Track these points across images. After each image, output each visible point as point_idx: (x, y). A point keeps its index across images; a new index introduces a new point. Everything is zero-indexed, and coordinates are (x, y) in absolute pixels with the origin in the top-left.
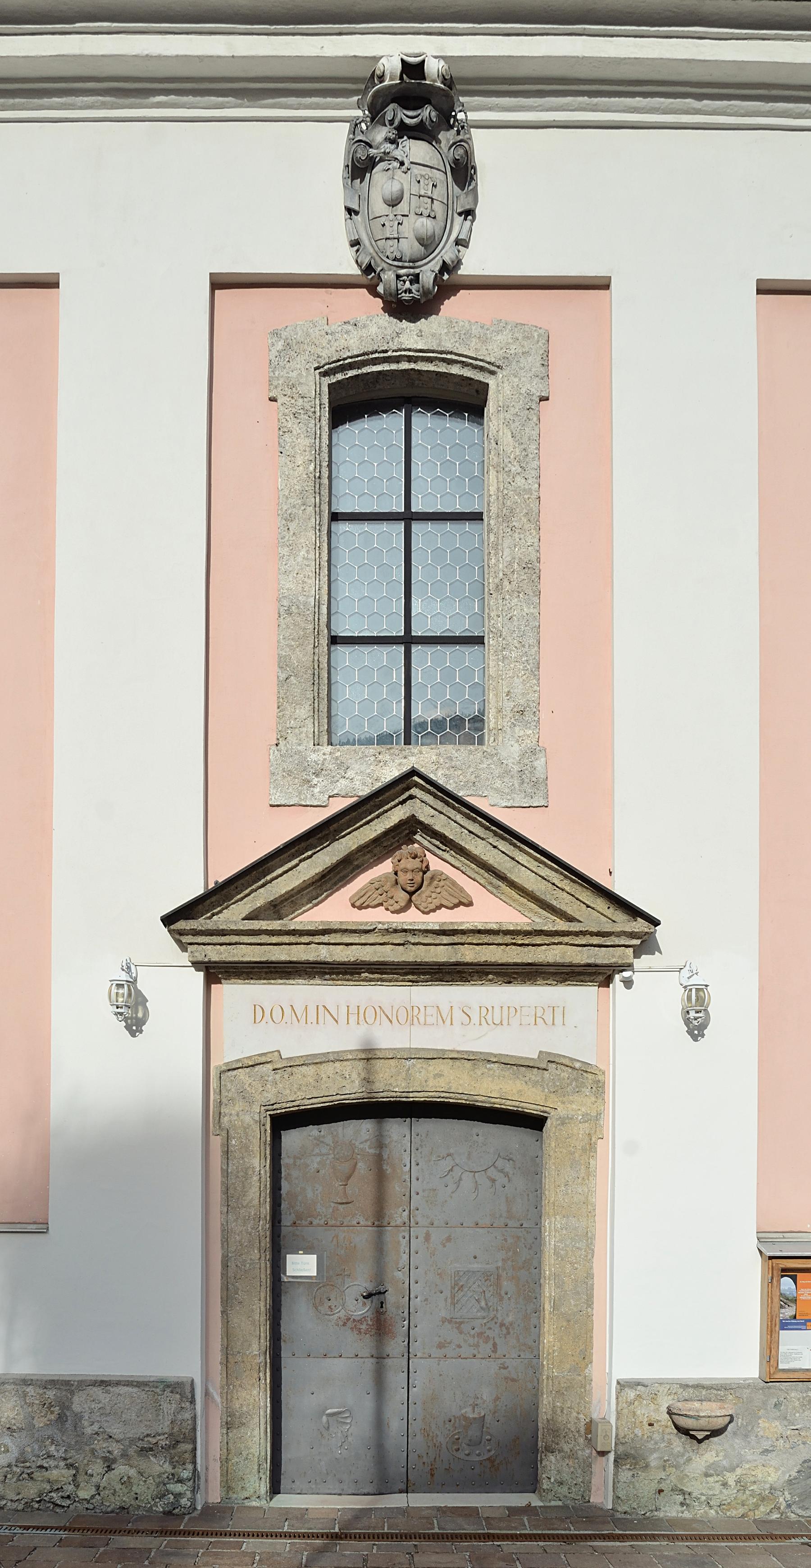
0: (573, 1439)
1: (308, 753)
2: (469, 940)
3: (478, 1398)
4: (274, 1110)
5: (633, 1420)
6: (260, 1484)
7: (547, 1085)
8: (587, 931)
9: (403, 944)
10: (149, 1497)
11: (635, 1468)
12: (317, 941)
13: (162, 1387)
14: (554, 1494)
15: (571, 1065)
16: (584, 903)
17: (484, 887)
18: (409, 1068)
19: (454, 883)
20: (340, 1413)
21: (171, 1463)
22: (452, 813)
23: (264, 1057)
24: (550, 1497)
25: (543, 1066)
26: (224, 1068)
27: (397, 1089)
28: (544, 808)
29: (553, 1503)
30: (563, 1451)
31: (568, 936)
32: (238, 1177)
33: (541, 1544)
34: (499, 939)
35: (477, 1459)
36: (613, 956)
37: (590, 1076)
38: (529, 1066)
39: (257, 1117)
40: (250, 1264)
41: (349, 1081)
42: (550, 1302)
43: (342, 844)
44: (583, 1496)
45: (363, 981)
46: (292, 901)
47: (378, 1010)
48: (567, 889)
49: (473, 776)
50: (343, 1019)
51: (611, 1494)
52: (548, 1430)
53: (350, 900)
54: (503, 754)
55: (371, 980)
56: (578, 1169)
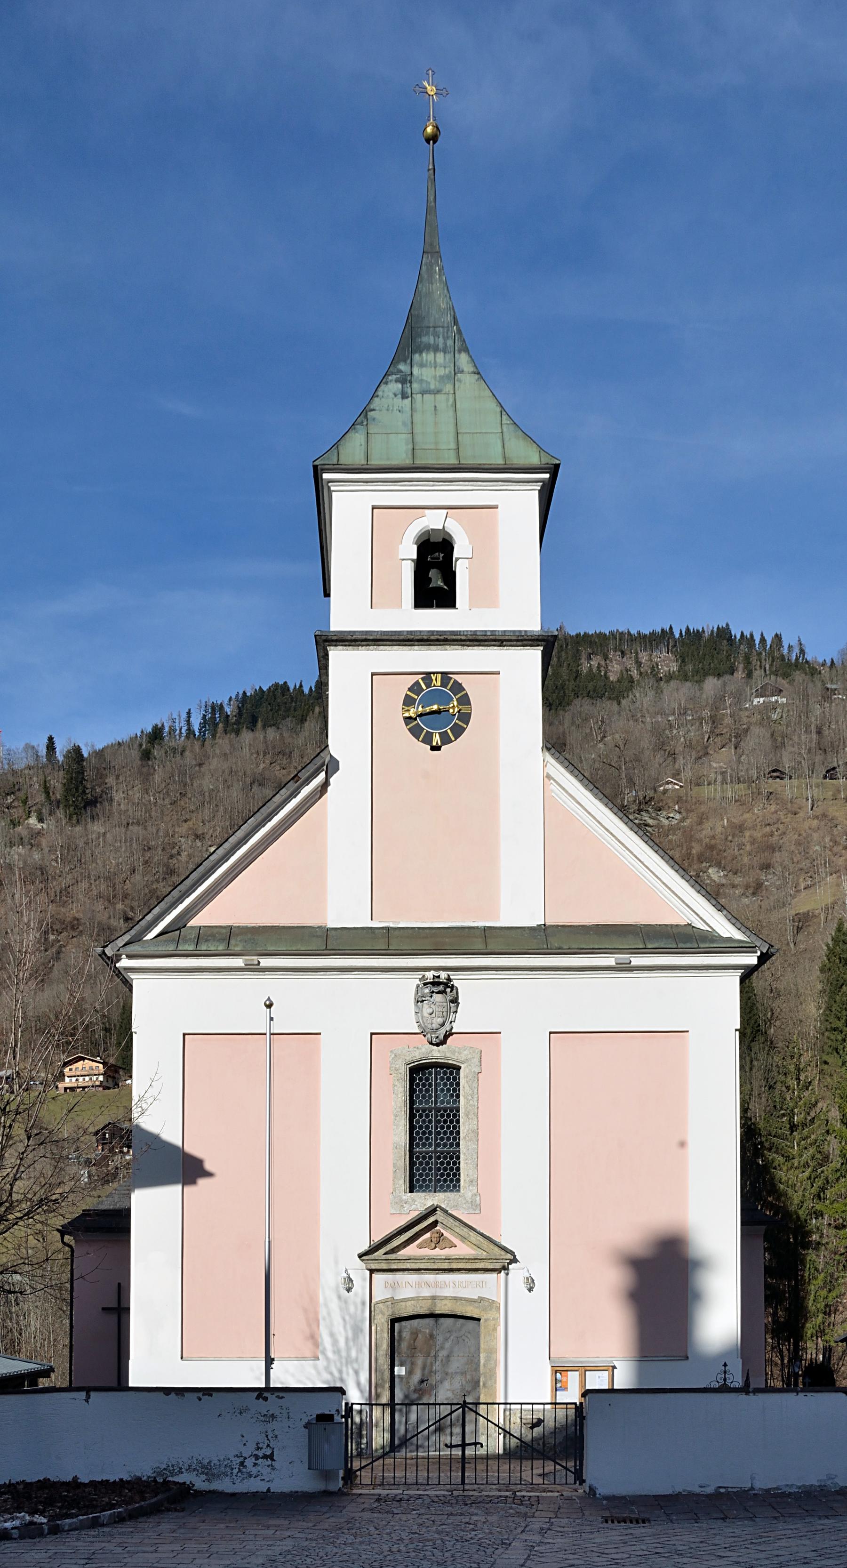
50: (414, 1286)
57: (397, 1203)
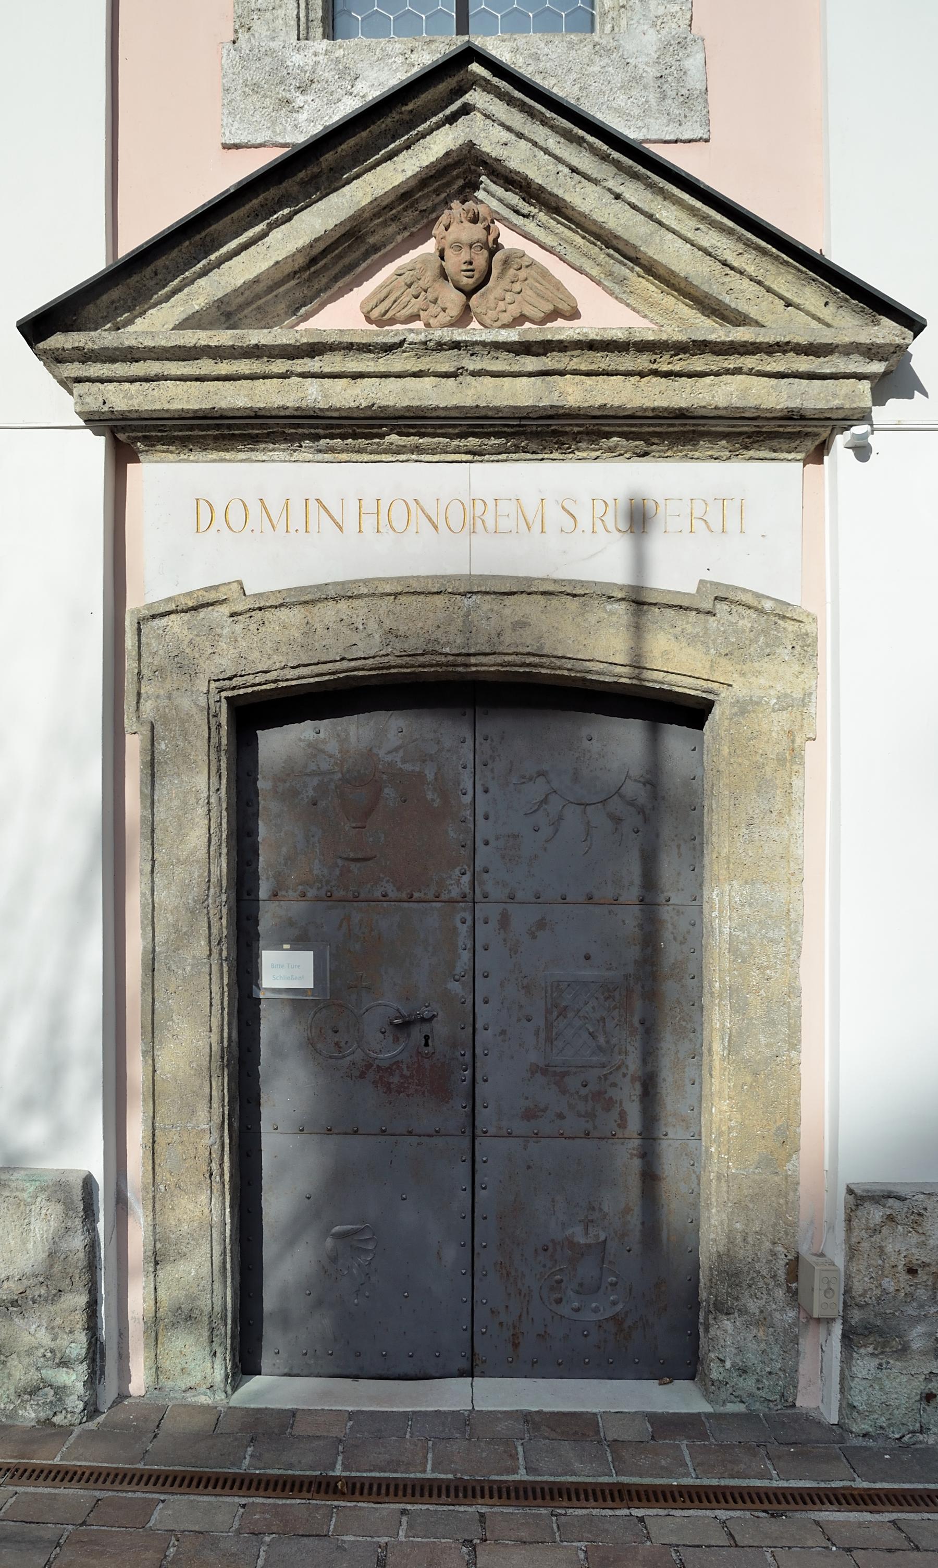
0: (765, 1292)
1: (287, 52)
2: (574, 364)
3: (593, 1209)
4: (234, 688)
5: (880, 1262)
6: (213, 1363)
7: (714, 641)
8: (788, 343)
9: (453, 375)
10: (12, 1391)
11: (882, 1353)
12: (299, 370)
13: (32, 1189)
14: (731, 1390)
15: (756, 604)
16: (781, 297)
17: (599, 283)
18: (469, 611)
19: (545, 274)
20: (356, 1232)
21: (50, 1329)
22: (540, 133)
23: (213, 592)
24: (723, 1396)
25: (707, 605)
26: (146, 612)
27: (447, 650)
28: (702, 144)
29: (731, 1408)
30: (747, 1312)
31: (753, 354)
32: (170, 808)
33: (722, 1514)
34: (627, 362)
35: (594, 1317)
36: (835, 395)
37: (790, 626)
38: (681, 607)
39: (202, 701)
40: (193, 966)
41: (364, 634)
42: (723, 1039)
43: (344, 195)
44: (783, 1395)
45: (385, 452)
46: (259, 308)
47: (412, 505)
48: (751, 269)
49: (576, 87)
50: (351, 523)
51: (835, 1397)
52: (720, 1272)
53: (361, 307)
54: (629, 46)
55: (400, 450)
56: (770, 795)
57: (256, 88)
